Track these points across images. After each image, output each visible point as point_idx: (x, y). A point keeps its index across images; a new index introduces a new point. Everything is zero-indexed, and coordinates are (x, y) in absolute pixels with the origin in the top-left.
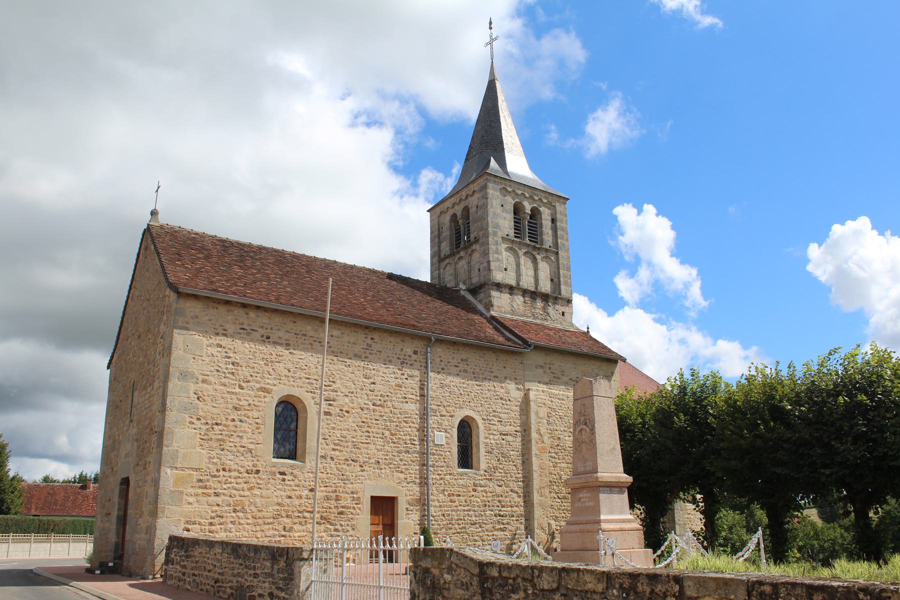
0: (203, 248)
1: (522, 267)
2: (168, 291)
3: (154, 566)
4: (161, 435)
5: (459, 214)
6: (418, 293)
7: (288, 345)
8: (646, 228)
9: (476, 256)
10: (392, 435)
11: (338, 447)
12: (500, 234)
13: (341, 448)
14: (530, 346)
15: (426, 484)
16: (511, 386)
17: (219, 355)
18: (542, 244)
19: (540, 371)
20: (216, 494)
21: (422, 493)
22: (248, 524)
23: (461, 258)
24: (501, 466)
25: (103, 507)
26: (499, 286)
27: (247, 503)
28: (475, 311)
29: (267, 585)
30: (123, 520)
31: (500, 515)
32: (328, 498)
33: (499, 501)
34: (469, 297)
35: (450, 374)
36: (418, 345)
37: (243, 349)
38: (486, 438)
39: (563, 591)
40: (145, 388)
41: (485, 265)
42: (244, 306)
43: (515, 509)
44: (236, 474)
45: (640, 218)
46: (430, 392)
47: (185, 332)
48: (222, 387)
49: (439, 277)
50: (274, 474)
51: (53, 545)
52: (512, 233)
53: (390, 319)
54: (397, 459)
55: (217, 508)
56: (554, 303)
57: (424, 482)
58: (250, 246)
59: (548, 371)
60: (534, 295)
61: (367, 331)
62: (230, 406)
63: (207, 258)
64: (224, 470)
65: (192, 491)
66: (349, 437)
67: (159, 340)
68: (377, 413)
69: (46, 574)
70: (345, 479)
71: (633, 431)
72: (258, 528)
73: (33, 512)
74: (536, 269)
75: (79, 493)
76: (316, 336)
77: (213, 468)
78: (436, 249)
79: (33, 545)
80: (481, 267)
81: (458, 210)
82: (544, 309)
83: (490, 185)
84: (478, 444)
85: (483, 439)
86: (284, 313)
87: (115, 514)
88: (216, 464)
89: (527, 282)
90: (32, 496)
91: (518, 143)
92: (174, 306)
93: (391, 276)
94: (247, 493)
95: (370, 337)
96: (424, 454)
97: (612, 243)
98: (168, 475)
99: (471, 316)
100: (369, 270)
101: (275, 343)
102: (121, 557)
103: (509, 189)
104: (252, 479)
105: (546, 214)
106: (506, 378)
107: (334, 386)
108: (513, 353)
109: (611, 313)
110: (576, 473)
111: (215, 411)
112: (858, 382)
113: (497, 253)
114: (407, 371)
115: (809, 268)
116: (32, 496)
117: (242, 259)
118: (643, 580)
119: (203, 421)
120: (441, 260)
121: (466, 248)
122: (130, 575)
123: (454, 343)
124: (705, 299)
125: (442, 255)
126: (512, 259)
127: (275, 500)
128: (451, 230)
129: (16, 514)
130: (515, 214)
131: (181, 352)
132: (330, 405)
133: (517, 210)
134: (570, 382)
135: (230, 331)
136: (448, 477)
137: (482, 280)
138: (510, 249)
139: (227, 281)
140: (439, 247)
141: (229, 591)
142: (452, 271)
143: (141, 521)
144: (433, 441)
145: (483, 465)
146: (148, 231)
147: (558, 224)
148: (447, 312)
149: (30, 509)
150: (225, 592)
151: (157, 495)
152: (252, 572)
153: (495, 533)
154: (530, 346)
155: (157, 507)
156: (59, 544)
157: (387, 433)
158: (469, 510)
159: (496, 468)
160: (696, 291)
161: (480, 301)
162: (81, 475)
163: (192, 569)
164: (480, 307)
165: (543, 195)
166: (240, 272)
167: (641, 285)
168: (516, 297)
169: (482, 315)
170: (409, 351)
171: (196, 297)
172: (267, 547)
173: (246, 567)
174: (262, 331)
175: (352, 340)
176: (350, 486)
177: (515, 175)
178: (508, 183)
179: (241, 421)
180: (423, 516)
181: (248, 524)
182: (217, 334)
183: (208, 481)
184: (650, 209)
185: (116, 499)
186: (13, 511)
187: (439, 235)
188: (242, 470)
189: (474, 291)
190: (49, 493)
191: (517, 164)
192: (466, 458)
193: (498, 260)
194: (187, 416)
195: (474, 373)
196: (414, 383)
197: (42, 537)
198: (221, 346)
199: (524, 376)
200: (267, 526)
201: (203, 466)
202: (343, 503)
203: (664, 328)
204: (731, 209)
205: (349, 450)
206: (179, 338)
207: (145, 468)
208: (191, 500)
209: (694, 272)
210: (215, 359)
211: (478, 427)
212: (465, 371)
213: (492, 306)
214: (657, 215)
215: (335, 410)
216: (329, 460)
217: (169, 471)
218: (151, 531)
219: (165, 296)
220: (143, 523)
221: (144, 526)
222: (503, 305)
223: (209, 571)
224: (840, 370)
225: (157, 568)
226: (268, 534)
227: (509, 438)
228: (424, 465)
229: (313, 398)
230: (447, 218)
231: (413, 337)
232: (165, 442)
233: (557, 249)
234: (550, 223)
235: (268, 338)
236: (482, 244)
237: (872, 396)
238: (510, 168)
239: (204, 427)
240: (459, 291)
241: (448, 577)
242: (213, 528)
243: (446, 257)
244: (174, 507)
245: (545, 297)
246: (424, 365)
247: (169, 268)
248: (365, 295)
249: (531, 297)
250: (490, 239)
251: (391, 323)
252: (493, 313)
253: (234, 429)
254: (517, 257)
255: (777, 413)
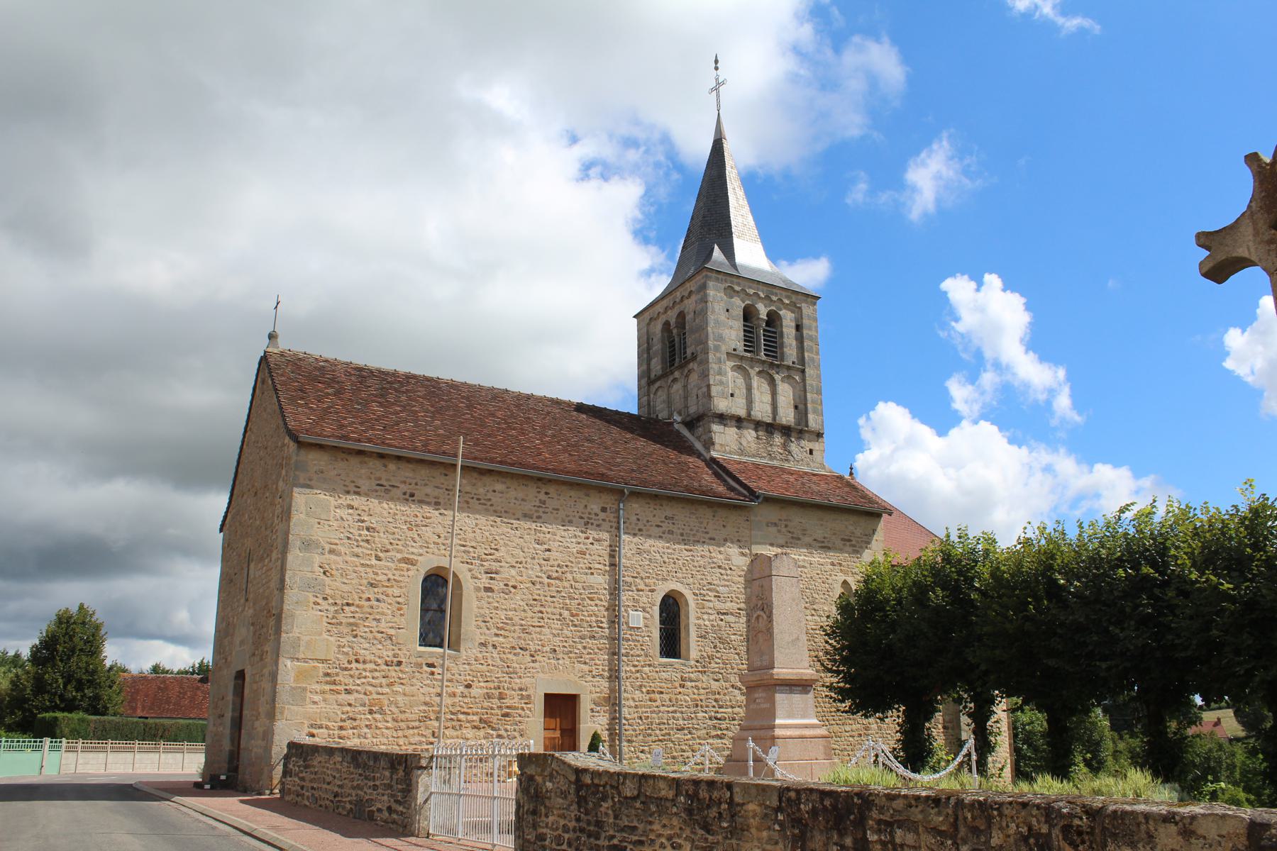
0: (333, 380)
1: (755, 392)
2: (287, 440)
3: (271, 778)
4: (279, 618)
5: (673, 322)
6: (615, 430)
7: (437, 504)
8: (991, 309)
9: (694, 378)
10: (572, 615)
11: (502, 632)
12: (724, 348)
13: (506, 633)
14: (758, 497)
15: (617, 678)
16: (733, 550)
17: (350, 518)
18: (782, 360)
19: (773, 530)
20: (348, 692)
21: (612, 690)
22: (387, 728)
23: (675, 380)
24: (718, 655)
25: (216, 707)
26: (722, 418)
27: (386, 702)
28: (691, 451)
29: (386, 798)
30: (238, 723)
31: (716, 718)
32: (489, 696)
33: (716, 700)
34: (685, 432)
35: (650, 536)
36: (608, 500)
37: (381, 510)
38: (698, 618)
39: (643, 799)
40: (262, 559)
41: (705, 389)
42: (382, 456)
43: (737, 710)
44: (372, 666)
45: (981, 295)
46: (623, 560)
47: (308, 491)
48: (355, 559)
49: (649, 404)
50: (420, 666)
51: (163, 756)
52: (740, 346)
53: (572, 467)
54: (580, 646)
55: (348, 708)
56: (799, 438)
57: (614, 675)
58: (395, 374)
59: (784, 530)
60: (770, 428)
61: (540, 484)
62: (365, 582)
63: (338, 393)
64: (357, 661)
65: (318, 687)
66: (516, 619)
67: (278, 500)
68: (553, 588)
69: (146, 789)
70: (511, 673)
71: (883, 609)
72: (400, 733)
73: (139, 713)
74: (774, 394)
75: (198, 688)
76: (474, 491)
77: (344, 660)
78: (645, 367)
79: (138, 756)
80: (700, 393)
81: (672, 316)
82: (785, 446)
83: (711, 284)
84: (687, 625)
85: (695, 620)
86: (432, 464)
87: (229, 715)
88: (347, 654)
89: (762, 411)
90: (138, 691)
91: (752, 223)
92: (294, 458)
93: (581, 408)
94: (386, 690)
95: (543, 491)
96: (615, 640)
97: (942, 334)
98: (288, 669)
99: (684, 458)
100: (552, 400)
101: (421, 502)
102: (236, 769)
103: (737, 288)
104: (393, 672)
105: (788, 318)
106: (726, 540)
107: (497, 554)
108: (736, 507)
109: (942, 432)
110: (751, 669)
111: (346, 588)
112: (1148, 550)
113: (720, 373)
114: (593, 534)
115: (1229, 364)
116: (138, 691)
117: (383, 393)
118: (703, 786)
119: (331, 601)
120: (651, 383)
121: (681, 367)
122: (245, 791)
123: (656, 497)
124: (1079, 414)
125: (652, 376)
126: (740, 381)
127: (422, 698)
128: (663, 342)
129: (115, 715)
130: (746, 319)
131: (303, 516)
132: (491, 578)
133: (748, 315)
134: (814, 543)
135: (364, 489)
136: (647, 669)
137: (701, 411)
138: (738, 368)
139: (361, 424)
140: (649, 364)
141: (348, 806)
142: (664, 397)
143: (257, 724)
144: (627, 623)
145: (694, 654)
146: (264, 360)
147: (805, 332)
148: (651, 454)
149: (134, 709)
150: (344, 808)
151: (275, 692)
152: (371, 783)
153: (710, 741)
154: (758, 497)
155: (274, 707)
156: (170, 755)
157: (566, 614)
158: (675, 712)
159: (711, 657)
160: (1063, 402)
161: (698, 438)
162: (201, 664)
163: (311, 781)
164: (698, 446)
165: (784, 293)
166: (380, 410)
167: (983, 393)
168: (745, 432)
169: (699, 456)
170: (595, 507)
171: (321, 447)
172: (386, 754)
173: (366, 778)
174: (404, 488)
175: (520, 495)
176: (518, 681)
177: (745, 268)
178: (736, 280)
179: (378, 600)
180: (614, 719)
181: (387, 728)
182: (348, 492)
183: (337, 675)
184: (993, 280)
185: (230, 697)
186: (111, 711)
187: (649, 349)
188: (379, 661)
189: (691, 424)
190: (159, 688)
191: (750, 253)
192: (671, 644)
193: (721, 383)
194: (310, 595)
195: (682, 535)
196: (602, 550)
197: (148, 745)
198: (352, 508)
199: (750, 536)
200: (411, 731)
201: (331, 656)
202: (508, 702)
203: (1024, 450)
204: (1110, 284)
205: (516, 635)
206: (301, 499)
207: (262, 659)
208: (316, 698)
209: (1061, 373)
210: (346, 524)
211: (687, 604)
212: (671, 532)
213: (713, 444)
214: (1004, 290)
215: (498, 585)
216: (490, 648)
217: (289, 663)
218: (268, 735)
219: (284, 445)
220: (260, 726)
221: (261, 730)
222: (728, 443)
223: (329, 783)
224: (1132, 531)
225: (276, 781)
226: (412, 740)
227: (731, 618)
228: (614, 654)
229: (470, 570)
230: (658, 327)
231: (601, 490)
232: (284, 628)
233: (803, 365)
234: (794, 331)
235: (412, 495)
236: (700, 363)
237: (1161, 567)
238: (740, 258)
239: (332, 609)
240: (671, 424)
241: (549, 785)
242: (343, 732)
243: (658, 378)
244: (295, 708)
245: (786, 431)
246: (615, 525)
247: (289, 409)
248: (543, 435)
249: (767, 431)
250: (711, 356)
251: (574, 474)
252: (714, 454)
253: (369, 610)
254: (747, 378)
255: (1054, 591)
